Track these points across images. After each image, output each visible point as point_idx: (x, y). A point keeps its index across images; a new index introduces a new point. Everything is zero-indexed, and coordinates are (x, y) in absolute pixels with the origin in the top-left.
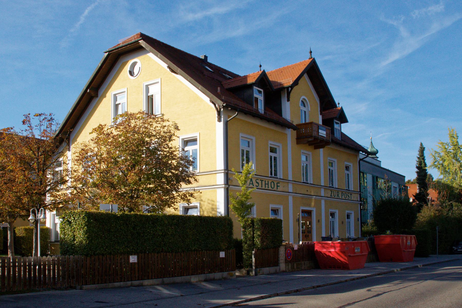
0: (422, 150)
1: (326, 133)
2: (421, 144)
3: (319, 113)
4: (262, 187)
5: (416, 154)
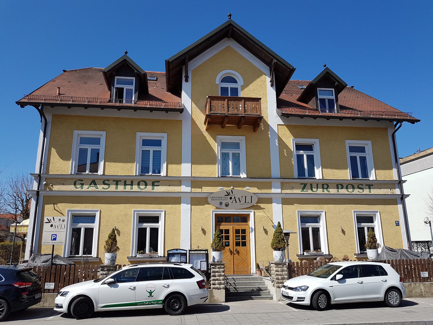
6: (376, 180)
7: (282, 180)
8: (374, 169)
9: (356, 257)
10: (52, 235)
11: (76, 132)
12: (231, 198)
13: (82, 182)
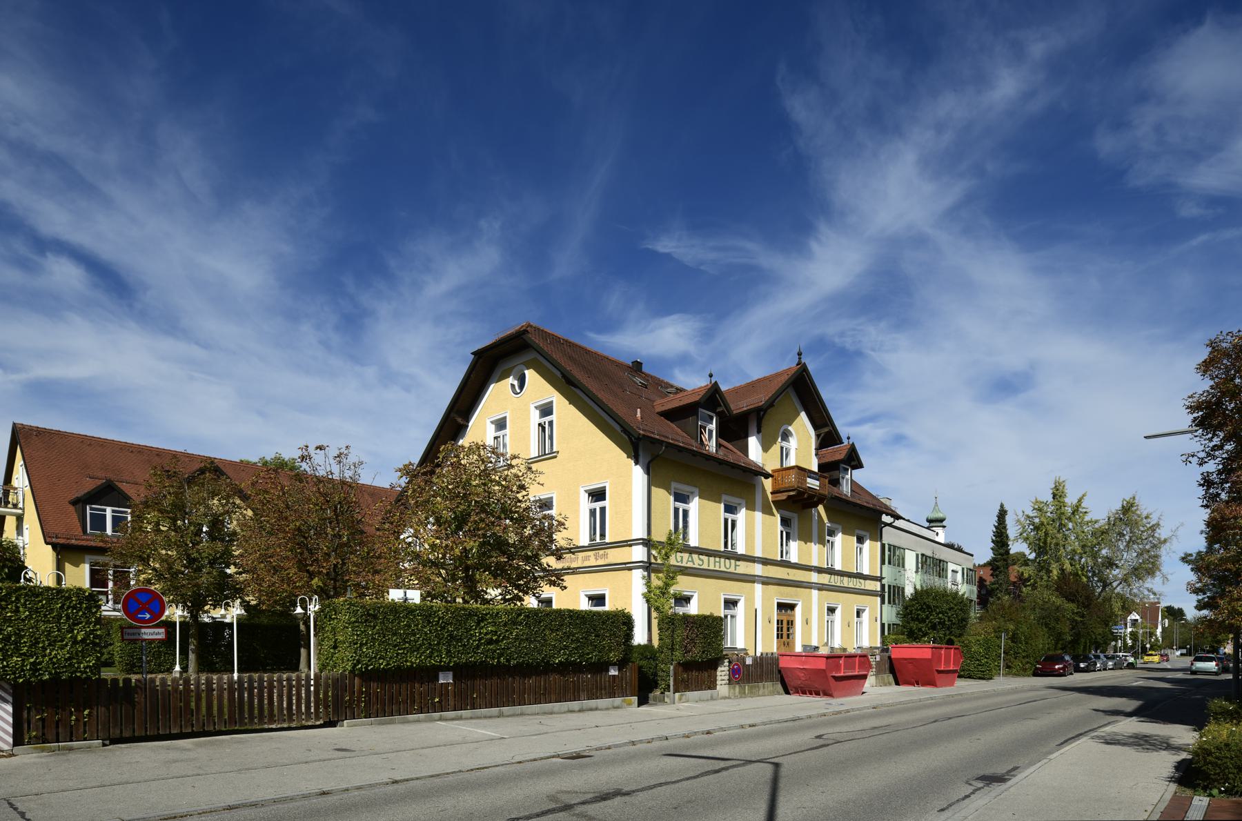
0: (1002, 514)
1: (820, 483)
2: (1002, 506)
3: (813, 452)
4: (709, 566)
5: (994, 520)
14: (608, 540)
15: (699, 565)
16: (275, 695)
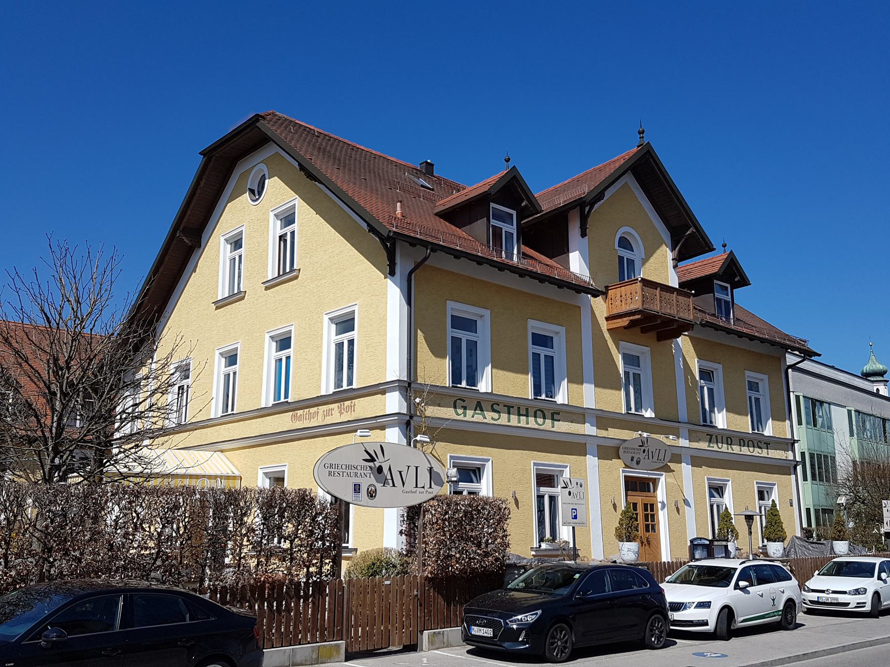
6: (491, 394)
7: (691, 427)
8: (490, 365)
9: (533, 555)
10: (572, 509)
11: (450, 304)
12: (644, 451)
13: (464, 404)
14: (354, 386)
15: (492, 419)
16: (9, 665)
